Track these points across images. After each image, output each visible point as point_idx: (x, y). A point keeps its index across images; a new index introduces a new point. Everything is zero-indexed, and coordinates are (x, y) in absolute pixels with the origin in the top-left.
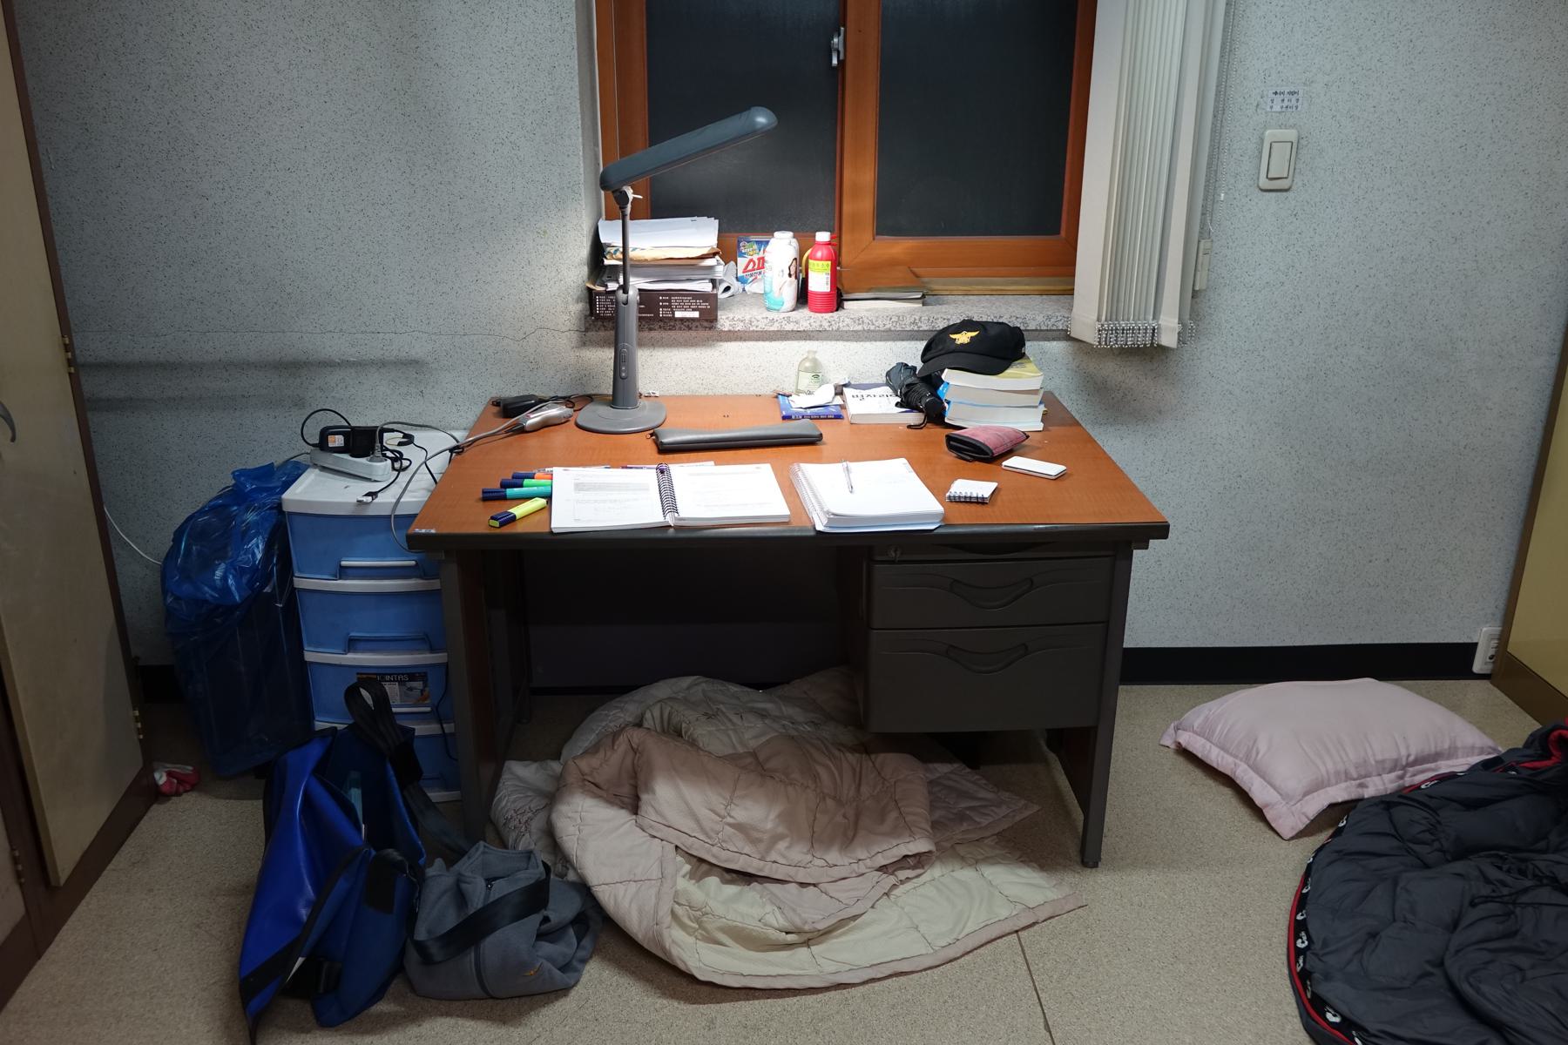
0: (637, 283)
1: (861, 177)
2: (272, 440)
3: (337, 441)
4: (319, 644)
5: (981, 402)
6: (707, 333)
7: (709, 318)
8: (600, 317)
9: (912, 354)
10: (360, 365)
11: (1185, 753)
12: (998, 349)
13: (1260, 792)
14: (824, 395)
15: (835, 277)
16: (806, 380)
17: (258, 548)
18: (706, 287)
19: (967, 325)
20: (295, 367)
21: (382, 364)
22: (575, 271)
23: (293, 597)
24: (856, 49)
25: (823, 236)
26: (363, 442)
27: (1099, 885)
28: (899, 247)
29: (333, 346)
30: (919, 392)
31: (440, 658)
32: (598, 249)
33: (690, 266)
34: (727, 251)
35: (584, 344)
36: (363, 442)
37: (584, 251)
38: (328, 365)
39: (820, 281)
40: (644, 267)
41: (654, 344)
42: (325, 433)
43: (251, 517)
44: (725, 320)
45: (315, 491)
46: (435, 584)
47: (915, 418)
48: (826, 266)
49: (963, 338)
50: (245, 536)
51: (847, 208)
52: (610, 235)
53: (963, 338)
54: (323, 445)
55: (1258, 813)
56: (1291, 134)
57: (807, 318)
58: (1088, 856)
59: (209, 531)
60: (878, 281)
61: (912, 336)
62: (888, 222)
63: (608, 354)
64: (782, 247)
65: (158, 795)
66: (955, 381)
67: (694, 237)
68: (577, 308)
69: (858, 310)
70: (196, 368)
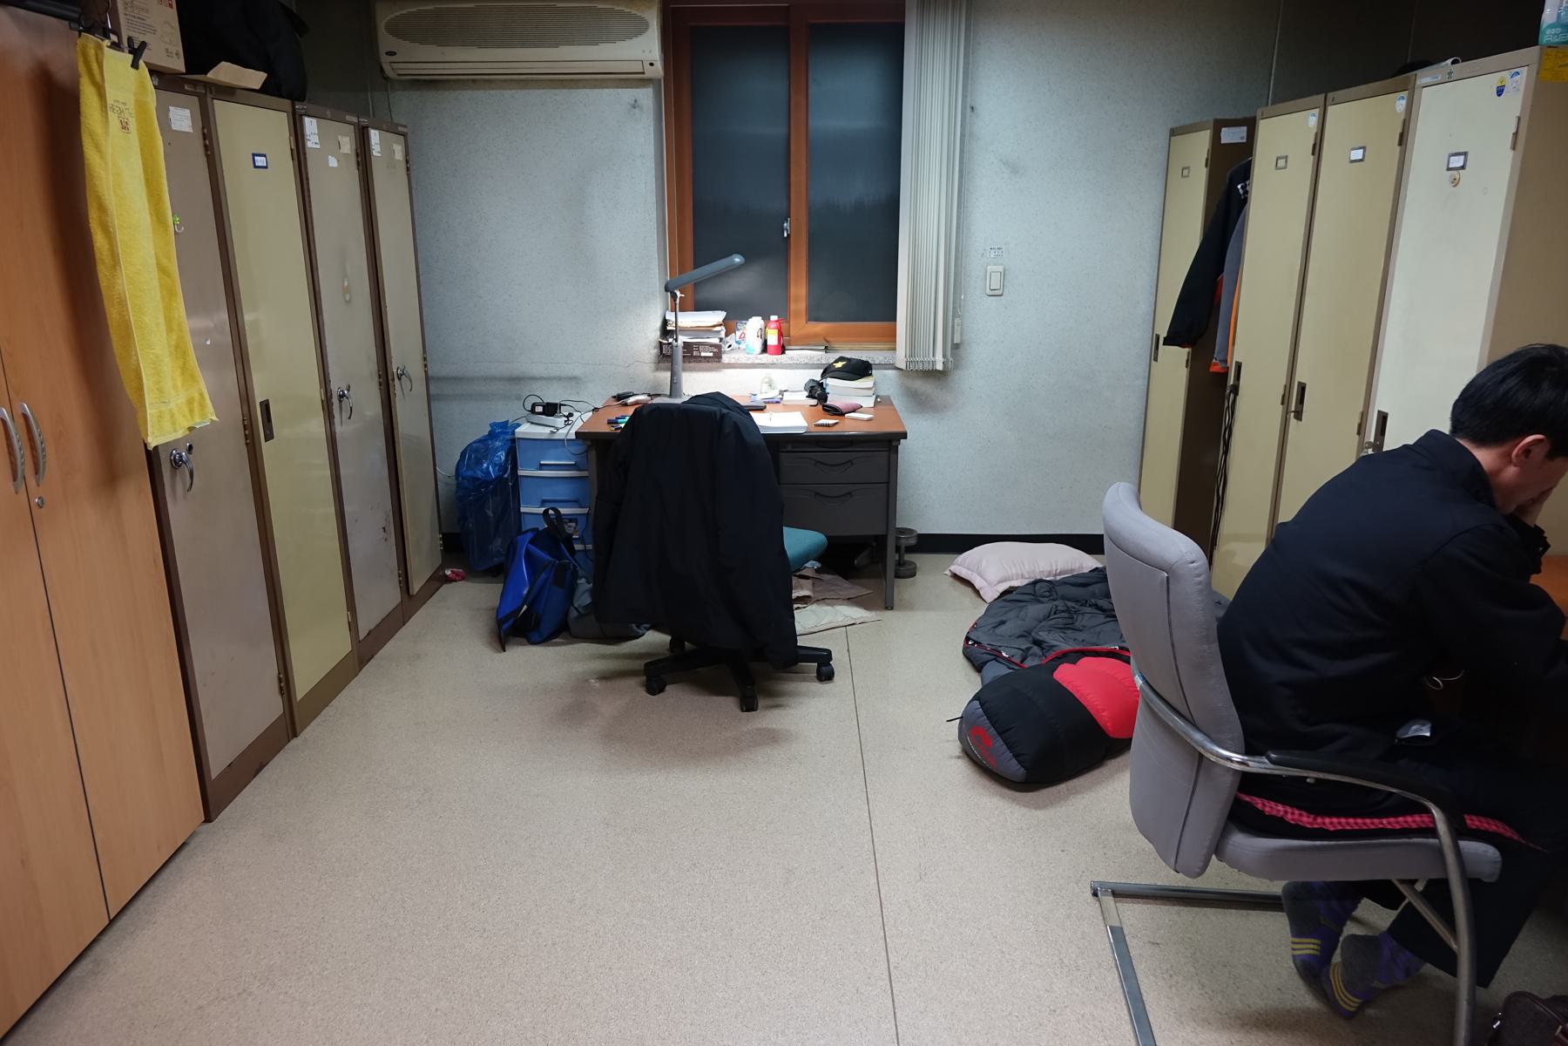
0: (682, 339)
1: (799, 291)
2: (504, 412)
3: (539, 409)
4: (528, 504)
5: (840, 391)
6: (715, 365)
7: (718, 356)
8: (665, 356)
9: (816, 375)
10: (548, 379)
11: (955, 576)
12: (859, 370)
13: (978, 583)
14: (774, 394)
15: (780, 335)
16: (765, 387)
17: (502, 455)
18: (716, 341)
19: (841, 359)
20: (516, 380)
21: (559, 379)
22: (654, 333)
23: (516, 478)
24: (795, 228)
25: (774, 318)
26: (551, 409)
27: (889, 613)
28: (820, 327)
29: (537, 370)
30: (817, 392)
31: (585, 511)
32: (665, 322)
33: (708, 330)
34: (729, 326)
35: (657, 370)
36: (551, 409)
37: (659, 324)
38: (534, 379)
39: (773, 340)
40: (685, 331)
41: (691, 370)
42: (534, 406)
43: (498, 444)
44: (726, 359)
45: (525, 430)
46: (585, 474)
47: (814, 402)
48: (776, 332)
49: (839, 365)
50: (497, 450)
51: (793, 307)
52: (670, 316)
53: (839, 365)
54: (533, 411)
55: (977, 592)
56: (1000, 268)
57: (766, 358)
58: (889, 606)
59: (475, 453)
60: (806, 342)
61: (817, 367)
62: (814, 315)
63: (669, 374)
64: (755, 323)
65: (448, 580)
66: (832, 384)
67: (715, 317)
68: (655, 351)
69: (792, 354)
70: (471, 380)
